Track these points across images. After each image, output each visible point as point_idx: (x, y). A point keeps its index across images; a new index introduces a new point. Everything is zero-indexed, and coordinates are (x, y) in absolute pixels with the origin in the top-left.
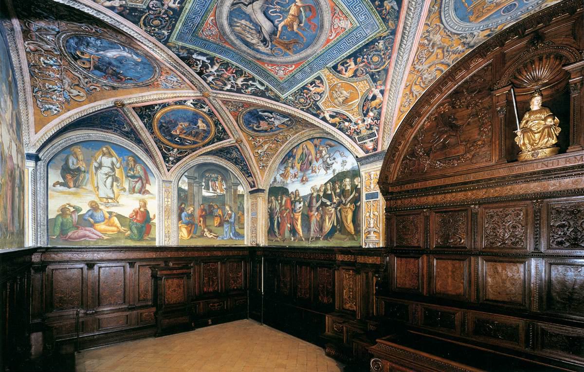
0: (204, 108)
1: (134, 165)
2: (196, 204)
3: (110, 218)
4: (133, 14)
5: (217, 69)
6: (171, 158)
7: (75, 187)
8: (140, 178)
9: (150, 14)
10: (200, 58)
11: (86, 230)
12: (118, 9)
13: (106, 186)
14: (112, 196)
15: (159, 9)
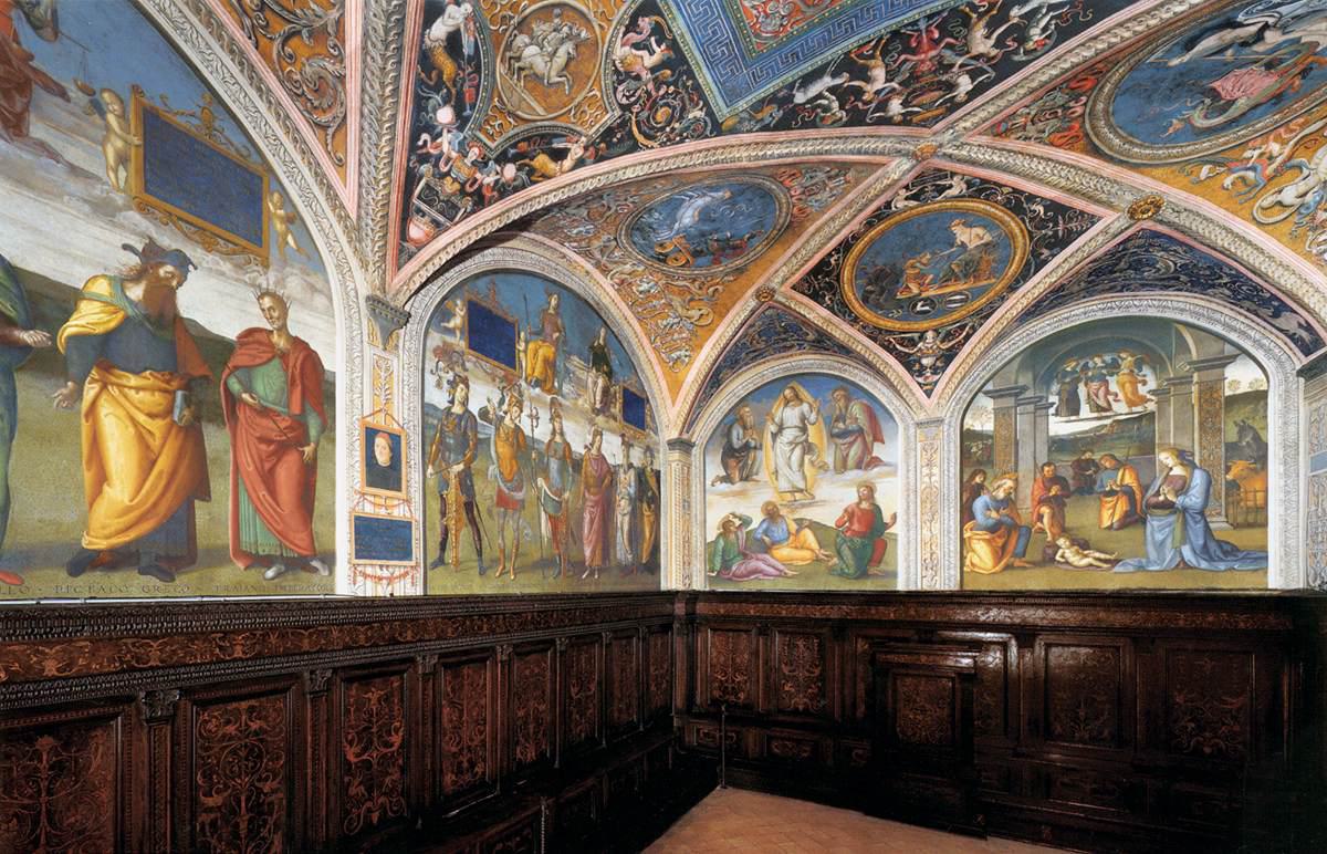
0: (951, 186)
1: (847, 408)
2: (1026, 466)
3: (798, 531)
4: (615, 140)
5: (887, 72)
6: (925, 361)
7: (741, 480)
8: (861, 431)
9: (637, 113)
10: (813, 90)
11: (757, 559)
12: (589, 157)
13: (790, 468)
14: (801, 485)
15: (639, 92)
